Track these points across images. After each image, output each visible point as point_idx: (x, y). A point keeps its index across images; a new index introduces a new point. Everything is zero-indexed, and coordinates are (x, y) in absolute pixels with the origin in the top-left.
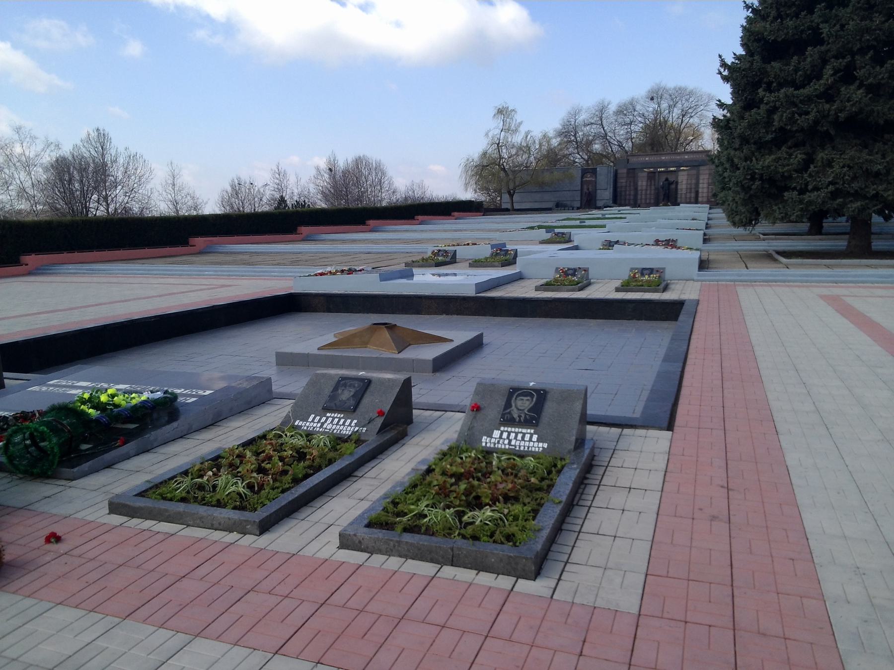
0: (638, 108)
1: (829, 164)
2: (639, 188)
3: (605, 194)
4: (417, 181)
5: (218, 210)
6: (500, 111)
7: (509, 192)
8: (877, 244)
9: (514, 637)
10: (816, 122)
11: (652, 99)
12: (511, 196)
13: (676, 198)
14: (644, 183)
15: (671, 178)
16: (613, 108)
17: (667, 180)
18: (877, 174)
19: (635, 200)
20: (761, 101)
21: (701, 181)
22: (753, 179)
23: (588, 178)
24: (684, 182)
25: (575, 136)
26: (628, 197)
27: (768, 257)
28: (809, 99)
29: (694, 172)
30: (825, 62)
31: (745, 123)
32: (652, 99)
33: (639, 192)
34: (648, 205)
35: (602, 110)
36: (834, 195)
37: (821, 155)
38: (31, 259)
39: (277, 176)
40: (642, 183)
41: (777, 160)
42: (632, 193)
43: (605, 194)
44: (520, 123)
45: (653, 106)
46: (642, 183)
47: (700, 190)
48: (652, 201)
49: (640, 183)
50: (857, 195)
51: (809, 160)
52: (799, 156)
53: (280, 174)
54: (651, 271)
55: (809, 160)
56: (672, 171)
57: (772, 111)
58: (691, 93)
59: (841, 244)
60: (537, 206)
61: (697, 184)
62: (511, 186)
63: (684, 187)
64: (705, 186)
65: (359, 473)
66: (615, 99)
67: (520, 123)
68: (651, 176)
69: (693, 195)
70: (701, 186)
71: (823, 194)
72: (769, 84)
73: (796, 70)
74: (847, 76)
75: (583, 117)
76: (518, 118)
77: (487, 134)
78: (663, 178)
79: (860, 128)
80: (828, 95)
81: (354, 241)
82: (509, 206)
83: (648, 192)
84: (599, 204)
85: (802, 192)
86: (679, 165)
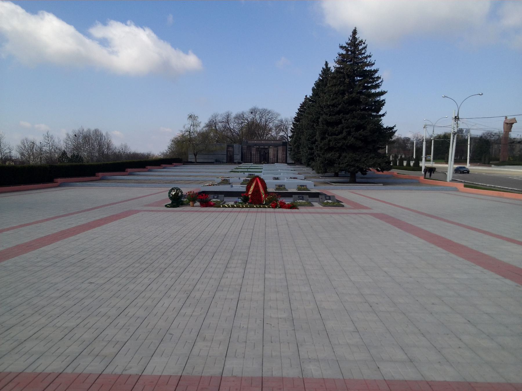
0: (245, 116)
1: (346, 157)
3: (237, 157)
4: (123, 143)
5: (19, 156)
6: (190, 117)
7: (195, 154)
8: (357, 180)
10: (342, 146)
11: (252, 113)
12: (195, 155)
13: (268, 160)
14: (255, 153)
16: (233, 115)
18: (357, 160)
19: (251, 160)
20: (327, 138)
22: (325, 160)
23: (230, 149)
25: (215, 127)
27: (327, 183)
28: (340, 139)
29: (276, 149)
30: (343, 129)
31: (322, 144)
32: (252, 113)
34: (273, 163)
35: (228, 116)
36: (347, 165)
37: (344, 154)
38: (59, 180)
39: (47, 138)
41: (332, 155)
43: (237, 157)
44: (200, 123)
45: (252, 116)
50: (353, 166)
51: (340, 156)
52: (337, 154)
53: (48, 136)
54: (303, 186)
55: (340, 156)
57: (330, 141)
58: (269, 112)
59: (348, 180)
60: (206, 161)
62: (195, 152)
63: (272, 155)
66: (235, 112)
67: (200, 123)
68: (257, 149)
69: (276, 159)
71: (345, 165)
72: (329, 133)
73: (336, 130)
74: (349, 133)
75: (219, 118)
76: (199, 120)
77: (184, 127)
79: (353, 148)
80: (345, 138)
81: (152, 175)
82: (193, 160)
84: (236, 161)
85: (339, 164)
86: (269, 146)
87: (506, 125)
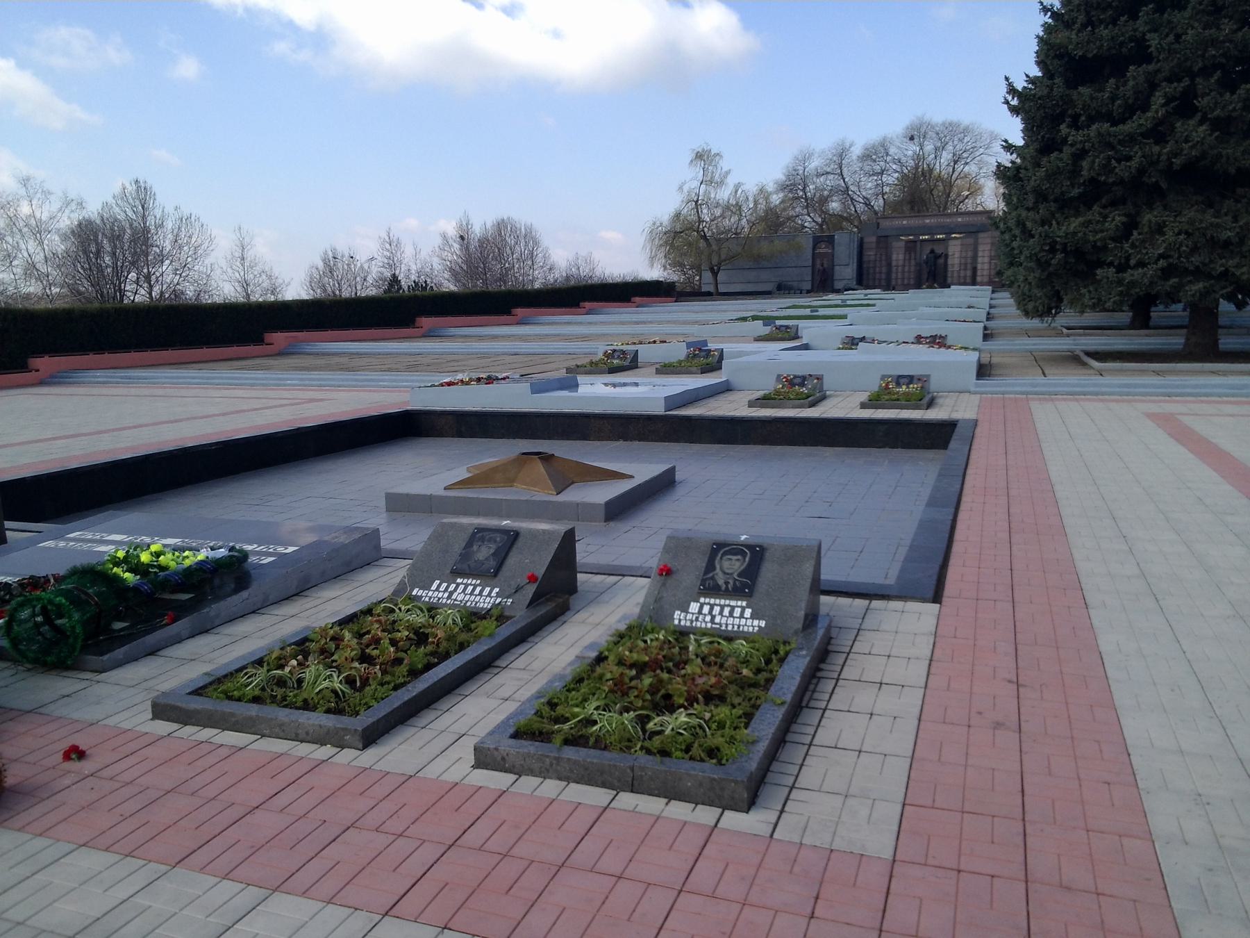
0: (892, 151)
1: (1160, 229)
2: (894, 263)
3: (846, 272)
4: (583, 253)
5: (304, 294)
6: (699, 156)
7: (712, 269)
8: (1227, 342)
9: (719, 892)
10: (1141, 171)
11: (912, 138)
12: (715, 274)
13: (945, 277)
14: (901, 257)
15: (939, 250)
16: (857, 151)
17: (932, 251)
18: (1227, 244)
19: (889, 279)
20: (1064, 141)
21: (980, 254)
22: (1053, 250)
23: (823, 249)
24: (957, 255)
25: (804, 190)
26: (877, 276)
27: (1074, 359)
28: (1131, 139)
29: (970, 241)
30: (1153, 86)
31: (1041, 173)
32: (912, 138)
33: (894, 269)
35: (842, 153)
36: (1166, 273)
37: (1148, 218)
38: (43, 363)
39: (388, 246)
40: (898, 256)
41: (1087, 224)
42: (884, 270)
43: (846, 272)
44: (728, 173)
45: (913, 148)
46: (898, 256)
47: (979, 266)
48: (912, 282)
49: (894, 257)
50: (1198, 274)
51: (1131, 225)
52: (1117, 219)
53: (392, 244)
54: (911, 379)
55: (1131, 225)
56: (939, 240)
57: (1080, 155)
58: (966, 131)
59: (1176, 341)
60: (750, 288)
61: (975, 257)
62: (715, 261)
63: (957, 261)
64: (986, 260)
65: (502, 662)
66: (860, 138)
67: (728, 173)
68: (911, 247)
69: (969, 273)
70: (980, 260)
71: (1150, 271)
72: (1076, 118)
73: (1113, 99)
74: (1184, 106)
75: (815, 164)
76: (724, 165)
77: (681, 188)
78: (927, 250)
79: (1203, 180)
80: (1158, 133)
81: (495, 338)
82: (711, 289)
83: (906, 269)
84: (838, 285)
85: (1122, 268)
86: (949, 231)
87: (816, 543)
